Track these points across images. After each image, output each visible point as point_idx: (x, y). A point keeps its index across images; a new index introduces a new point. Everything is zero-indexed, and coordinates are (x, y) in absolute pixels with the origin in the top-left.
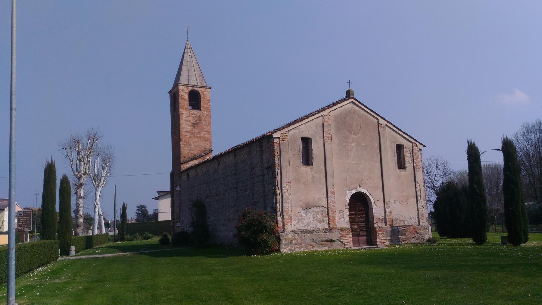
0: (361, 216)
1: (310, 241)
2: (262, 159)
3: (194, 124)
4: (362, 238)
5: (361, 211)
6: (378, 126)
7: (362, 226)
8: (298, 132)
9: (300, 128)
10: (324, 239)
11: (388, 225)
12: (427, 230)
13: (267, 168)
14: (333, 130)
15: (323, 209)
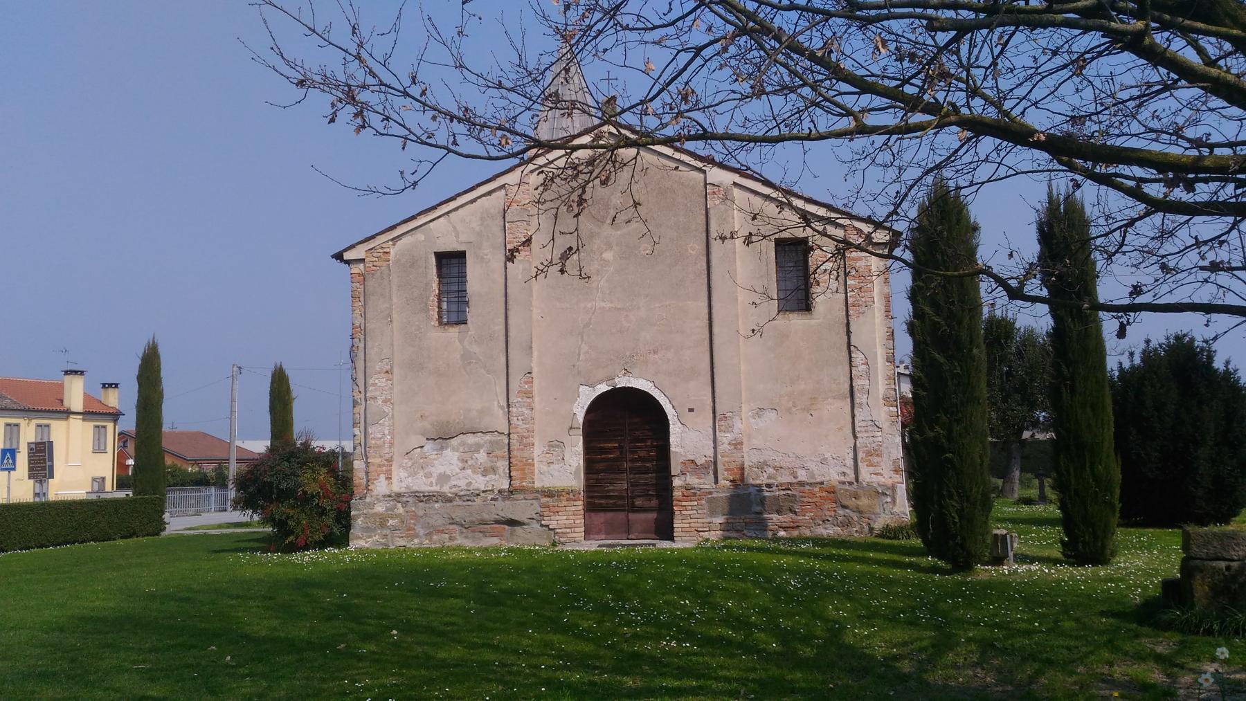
0: (642, 454)
1: (440, 521)
4: (642, 516)
5: (643, 441)
7: (646, 484)
8: (423, 239)
9: (431, 229)
10: (486, 517)
11: (722, 482)
12: (889, 499)
15: (493, 438)
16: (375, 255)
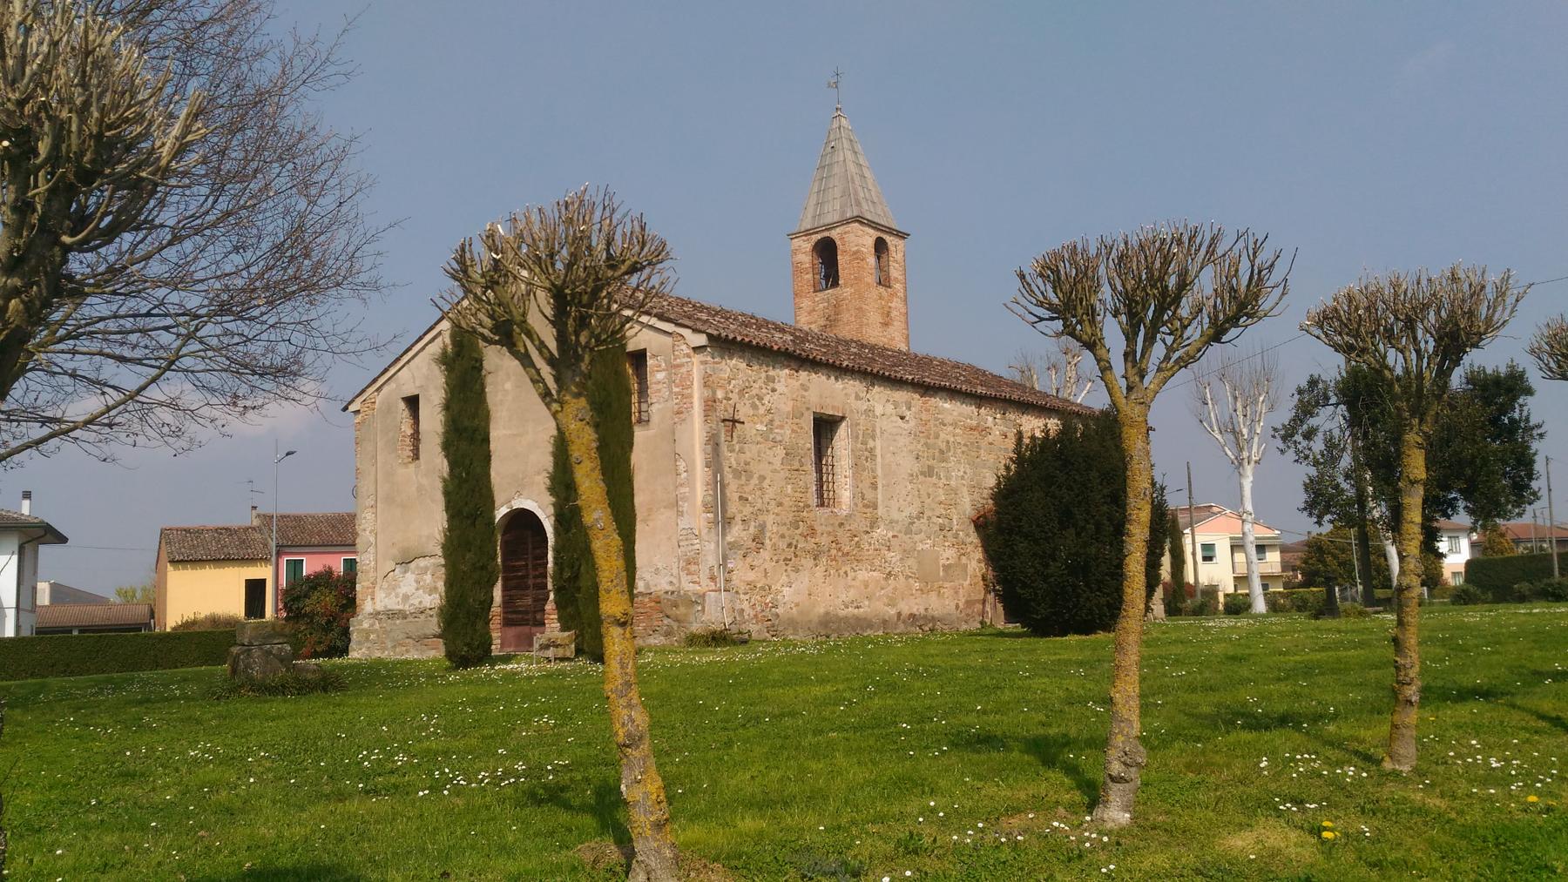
3: (825, 326)
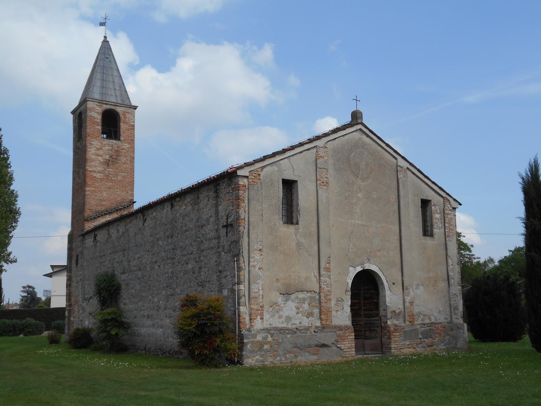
2: (217, 212)
3: (109, 160)
6: (396, 170)
8: (277, 169)
9: (281, 164)
13: (226, 226)
14: (331, 171)
15: (311, 295)
16: (254, 175)
